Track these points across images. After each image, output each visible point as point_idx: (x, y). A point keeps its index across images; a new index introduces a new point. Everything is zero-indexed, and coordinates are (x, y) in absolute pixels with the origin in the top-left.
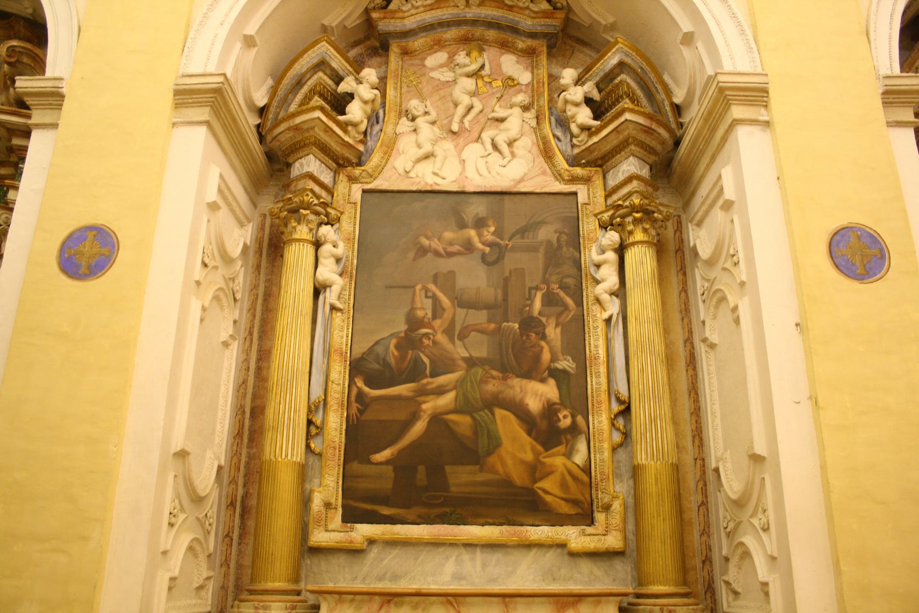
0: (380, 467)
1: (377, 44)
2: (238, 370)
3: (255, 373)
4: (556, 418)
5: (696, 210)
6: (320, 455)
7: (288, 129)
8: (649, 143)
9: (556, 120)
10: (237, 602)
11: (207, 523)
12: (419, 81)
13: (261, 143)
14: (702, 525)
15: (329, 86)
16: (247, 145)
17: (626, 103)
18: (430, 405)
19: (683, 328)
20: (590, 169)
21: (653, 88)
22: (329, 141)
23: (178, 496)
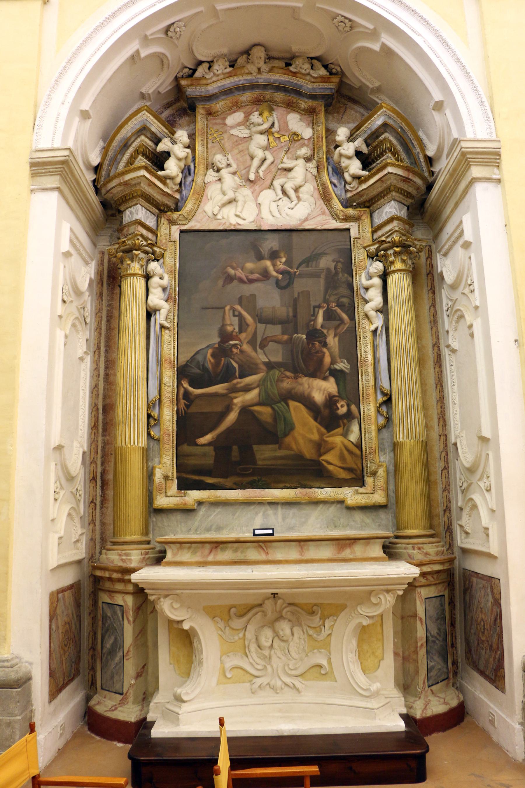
0: (204, 447)
1: (186, 105)
2: (92, 377)
3: (104, 378)
4: (335, 407)
5: (443, 244)
6: (158, 440)
7: (120, 184)
8: (407, 189)
9: (333, 169)
10: (104, 551)
11: (78, 494)
12: (222, 138)
13: (97, 195)
14: (444, 484)
15: (150, 146)
17: (389, 158)
18: (240, 400)
19: (432, 335)
20: (360, 209)
21: (411, 144)
22: (153, 193)
23: (58, 479)
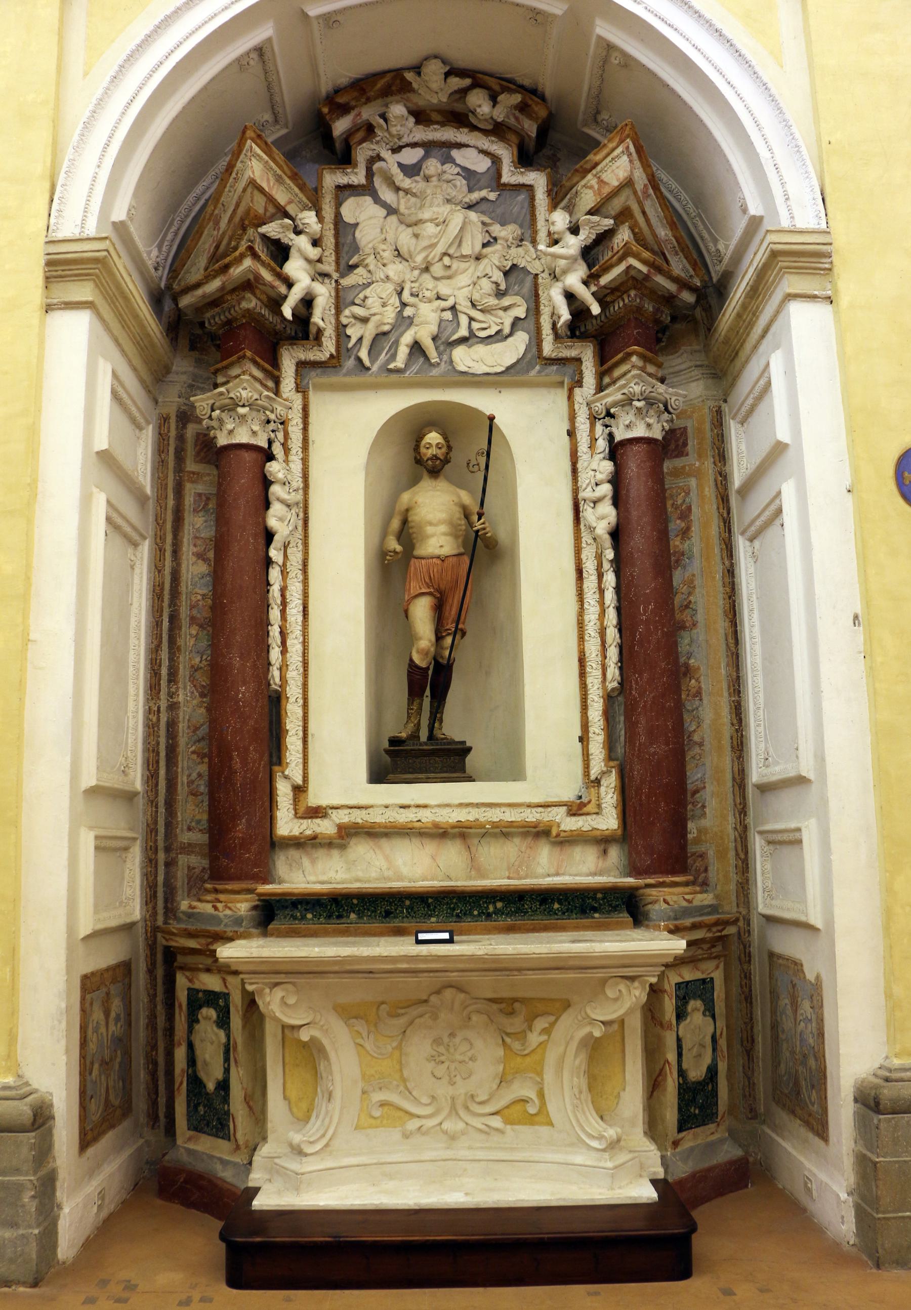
5: (743, 398)
16: (136, 317)
